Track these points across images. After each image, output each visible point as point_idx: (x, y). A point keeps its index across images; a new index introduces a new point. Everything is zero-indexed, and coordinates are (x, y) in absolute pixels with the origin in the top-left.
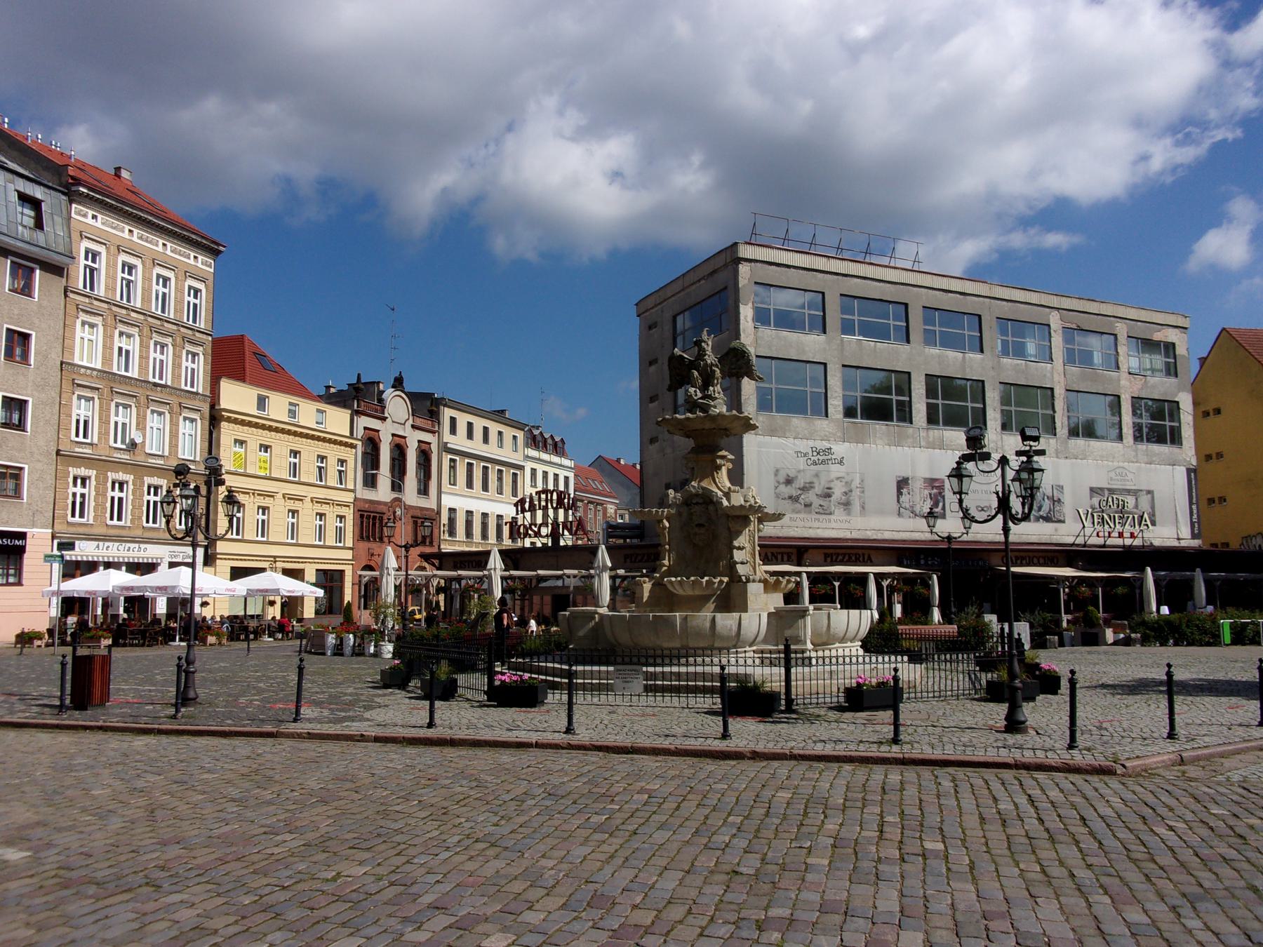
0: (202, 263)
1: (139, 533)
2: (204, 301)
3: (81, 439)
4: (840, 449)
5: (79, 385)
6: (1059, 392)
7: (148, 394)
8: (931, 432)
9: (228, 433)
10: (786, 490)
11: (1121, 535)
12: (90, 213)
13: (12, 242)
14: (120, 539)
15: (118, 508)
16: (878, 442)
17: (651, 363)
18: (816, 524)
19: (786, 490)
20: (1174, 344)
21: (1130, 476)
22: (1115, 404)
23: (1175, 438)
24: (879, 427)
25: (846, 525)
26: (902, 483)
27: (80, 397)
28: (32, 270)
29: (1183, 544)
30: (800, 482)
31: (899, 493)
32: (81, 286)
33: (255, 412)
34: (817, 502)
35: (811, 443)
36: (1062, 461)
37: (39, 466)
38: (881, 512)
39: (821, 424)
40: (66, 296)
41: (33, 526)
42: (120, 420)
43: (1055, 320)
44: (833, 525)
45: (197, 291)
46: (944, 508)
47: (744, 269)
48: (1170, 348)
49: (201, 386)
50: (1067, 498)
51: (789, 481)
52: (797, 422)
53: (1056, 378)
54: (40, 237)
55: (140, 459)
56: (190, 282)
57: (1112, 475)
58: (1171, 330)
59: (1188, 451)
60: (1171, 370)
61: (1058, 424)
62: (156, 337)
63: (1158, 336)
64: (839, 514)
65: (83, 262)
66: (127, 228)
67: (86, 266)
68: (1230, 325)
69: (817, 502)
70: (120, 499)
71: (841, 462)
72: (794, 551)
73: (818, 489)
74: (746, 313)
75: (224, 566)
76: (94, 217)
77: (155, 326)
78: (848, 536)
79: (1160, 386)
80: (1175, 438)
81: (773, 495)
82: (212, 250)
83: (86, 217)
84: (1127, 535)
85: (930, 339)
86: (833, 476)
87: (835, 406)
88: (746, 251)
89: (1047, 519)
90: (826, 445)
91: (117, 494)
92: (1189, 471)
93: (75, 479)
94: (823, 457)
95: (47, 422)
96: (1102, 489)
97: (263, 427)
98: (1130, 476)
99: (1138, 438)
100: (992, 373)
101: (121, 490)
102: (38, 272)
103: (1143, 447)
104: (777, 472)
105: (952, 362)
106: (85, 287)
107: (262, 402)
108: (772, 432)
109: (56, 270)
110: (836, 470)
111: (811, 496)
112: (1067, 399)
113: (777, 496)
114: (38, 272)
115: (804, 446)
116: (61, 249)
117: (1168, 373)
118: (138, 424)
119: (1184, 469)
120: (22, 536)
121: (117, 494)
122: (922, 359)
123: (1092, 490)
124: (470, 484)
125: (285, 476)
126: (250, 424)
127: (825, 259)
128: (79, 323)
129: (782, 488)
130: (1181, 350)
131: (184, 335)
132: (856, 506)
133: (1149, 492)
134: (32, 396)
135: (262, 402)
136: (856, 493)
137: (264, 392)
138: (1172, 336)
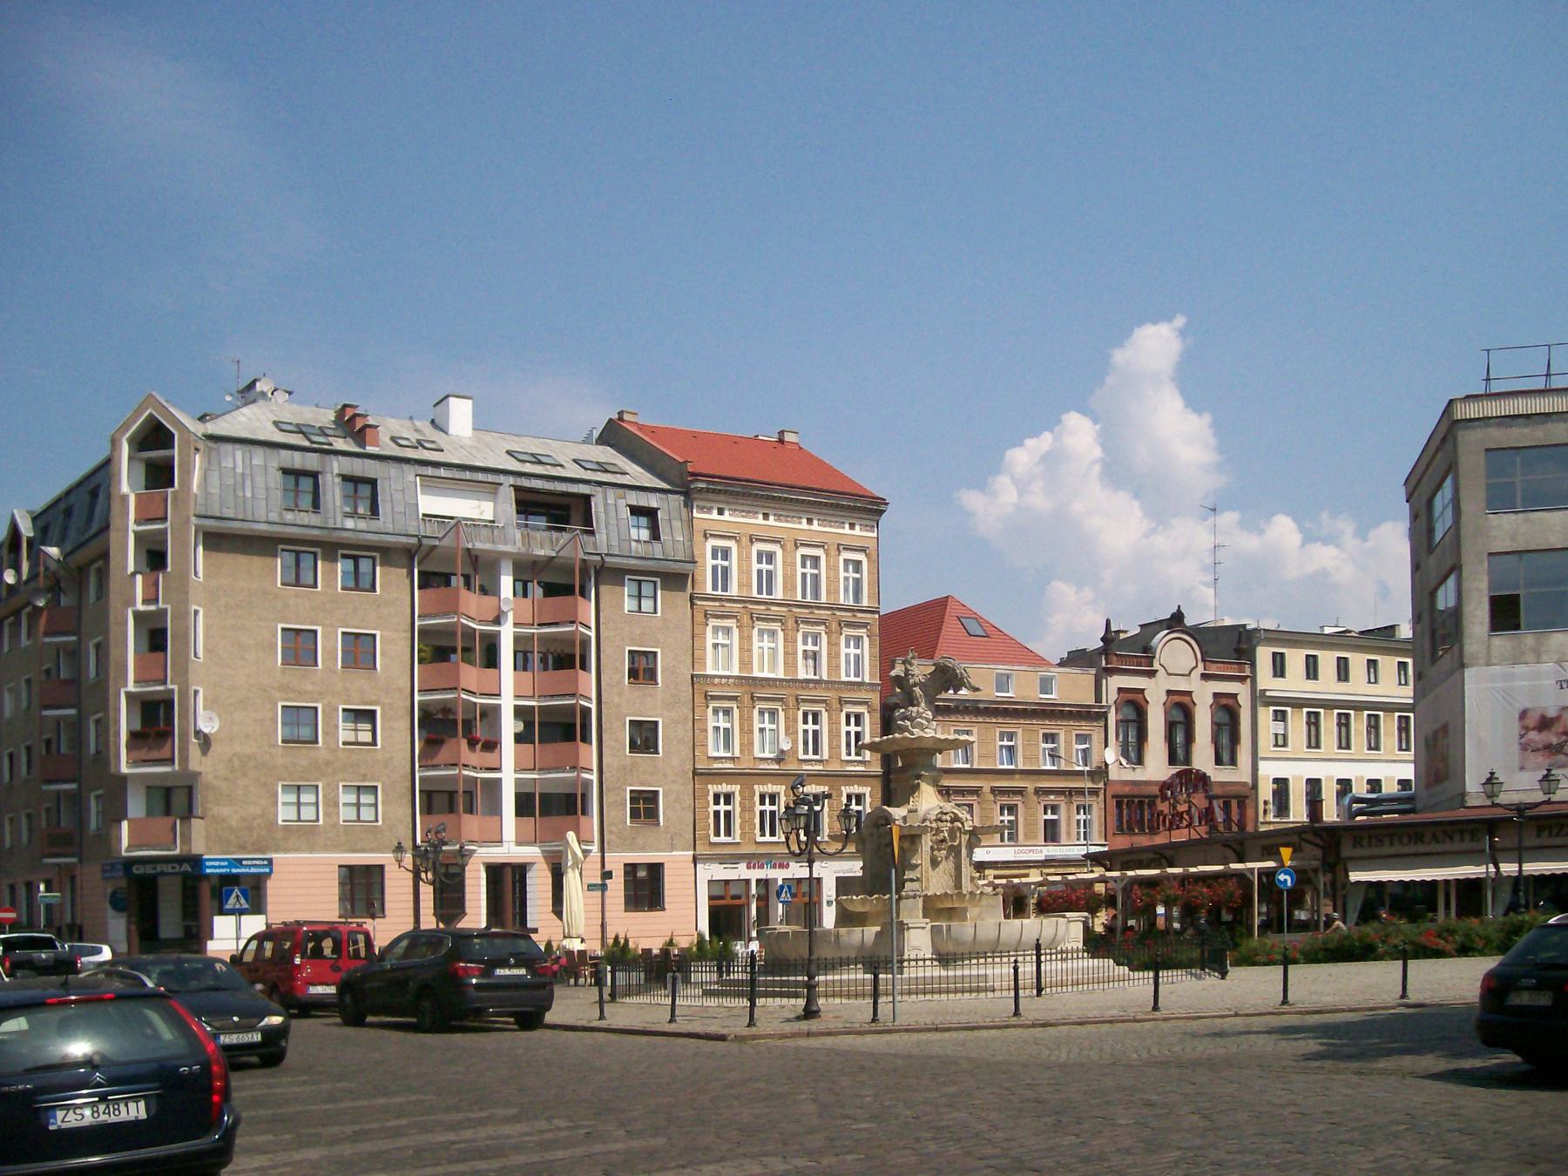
5: (804, 701)
37: (675, 787)
40: (692, 605)
54: (657, 550)
81: (1516, 747)
104: (1523, 715)
113: (1524, 747)
118: (787, 729)
124: (1374, 746)
129: (1533, 735)
134: (661, 716)
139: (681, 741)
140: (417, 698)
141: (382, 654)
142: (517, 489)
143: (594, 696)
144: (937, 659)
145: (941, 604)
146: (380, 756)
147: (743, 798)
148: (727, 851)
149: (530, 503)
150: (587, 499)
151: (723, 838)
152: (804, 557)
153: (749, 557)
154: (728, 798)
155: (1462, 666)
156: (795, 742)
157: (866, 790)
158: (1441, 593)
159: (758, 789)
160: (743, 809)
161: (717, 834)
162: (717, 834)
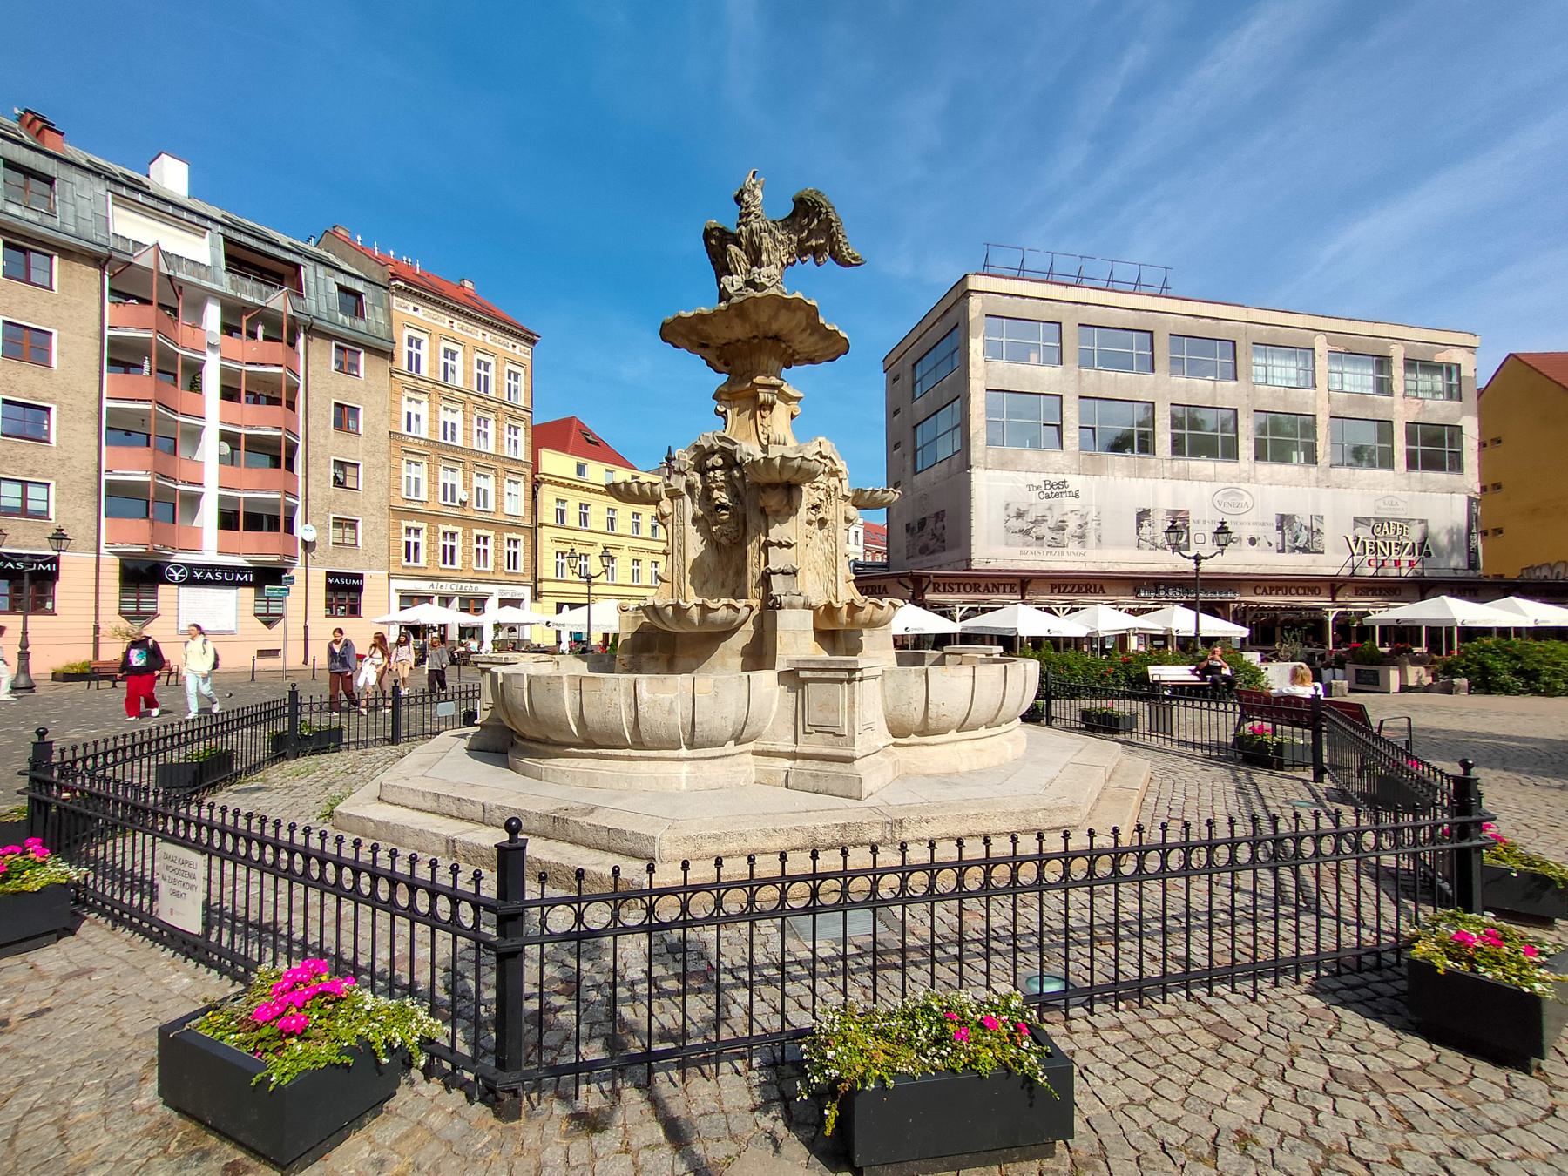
0: (520, 351)
1: (470, 575)
2: (522, 384)
3: (449, 502)
4: (1075, 482)
6: (1323, 421)
7: (497, 465)
8: (1175, 463)
9: (548, 495)
10: (1017, 524)
11: (1397, 563)
12: (412, 305)
13: (60, 236)
14: (449, 579)
15: (448, 554)
16: (1118, 474)
17: (895, 414)
18: (1049, 557)
19: (1017, 524)
20: (1459, 366)
21: (1401, 505)
22: (1385, 427)
23: (1457, 465)
24: (1118, 459)
25: (1081, 558)
26: (1143, 515)
27: (409, 463)
28: (51, 257)
29: (1460, 573)
30: (1031, 516)
31: (1139, 525)
32: (405, 368)
33: (575, 477)
34: (1049, 535)
35: (1044, 476)
36: (1324, 490)
37: (373, 519)
38: (1119, 545)
39: (1056, 457)
41: (370, 568)
42: (413, 476)
43: (1320, 344)
44: (1066, 557)
45: (517, 375)
46: (1188, 539)
47: (975, 303)
48: (1449, 369)
49: (523, 453)
50: (1327, 528)
51: (1020, 515)
52: (1030, 455)
53: (1320, 403)
54: (360, 325)
55: (469, 513)
56: (510, 367)
57: (1381, 504)
58: (1455, 350)
59: (1471, 478)
60: (1454, 393)
61: (1320, 453)
62: (509, 421)
63: (1439, 358)
64: (1073, 546)
65: (406, 348)
66: (448, 319)
67: (410, 354)
68: (1519, 349)
69: (1049, 535)
70: (452, 548)
71: (1076, 495)
72: (1018, 581)
73: (1051, 522)
74: (976, 346)
75: (549, 603)
76: (415, 309)
77: (479, 399)
78: (1083, 568)
79: (1440, 410)
80: (1457, 465)
82: (529, 339)
83: (403, 308)
84: (1404, 564)
85: (1177, 366)
86: (1068, 509)
87: (1071, 439)
88: (975, 283)
89: (1304, 550)
90: (1061, 477)
91: (513, 549)
92: (1470, 500)
93: (478, 537)
94: (1057, 489)
95: (379, 483)
96: (1368, 519)
97: (582, 489)
98: (1401, 505)
99: (1411, 464)
100: (1246, 401)
101: (485, 542)
102: (56, 259)
103: (1417, 474)
105: (1201, 389)
106: (410, 368)
107: (580, 469)
108: (1003, 466)
109: (384, 353)
110: (1070, 503)
111: (1043, 530)
112: (1332, 431)
113: (1008, 530)
114: (56, 259)
115: (1037, 479)
116: (383, 334)
117: (1450, 397)
119: (1464, 497)
120: (360, 577)
121: (513, 549)
122: (1167, 389)
123: (1356, 519)
125: (577, 525)
126: (569, 486)
127: (1062, 288)
128: (404, 399)
130: (1466, 372)
131: (508, 411)
132: (1092, 538)
133: (1422, 521)
135: (580, 469)
136: (1092, 526)
137: (582, 460)
138: (1455, 356)
139: (379, 483)
140: (106, 404)
141: (61, 353)
142: (227, 240)
143: (301, 433)
144: (781, 666)
145: (570, 421)
146: (54, 454)
147: (430, 533)
148: (416, 572)
149: (241, 259)
150: (297, 267)
151: (412, 563)
152: (479, 361)
153: (438, 352)
154: (417, 531)
155: (970, 467)
156: (471, 496)
157: (521, 537)
158: (387, 888)
159: (442, 528)
160: (429, 542)
161: (444, 562)
162: (444, 562)
